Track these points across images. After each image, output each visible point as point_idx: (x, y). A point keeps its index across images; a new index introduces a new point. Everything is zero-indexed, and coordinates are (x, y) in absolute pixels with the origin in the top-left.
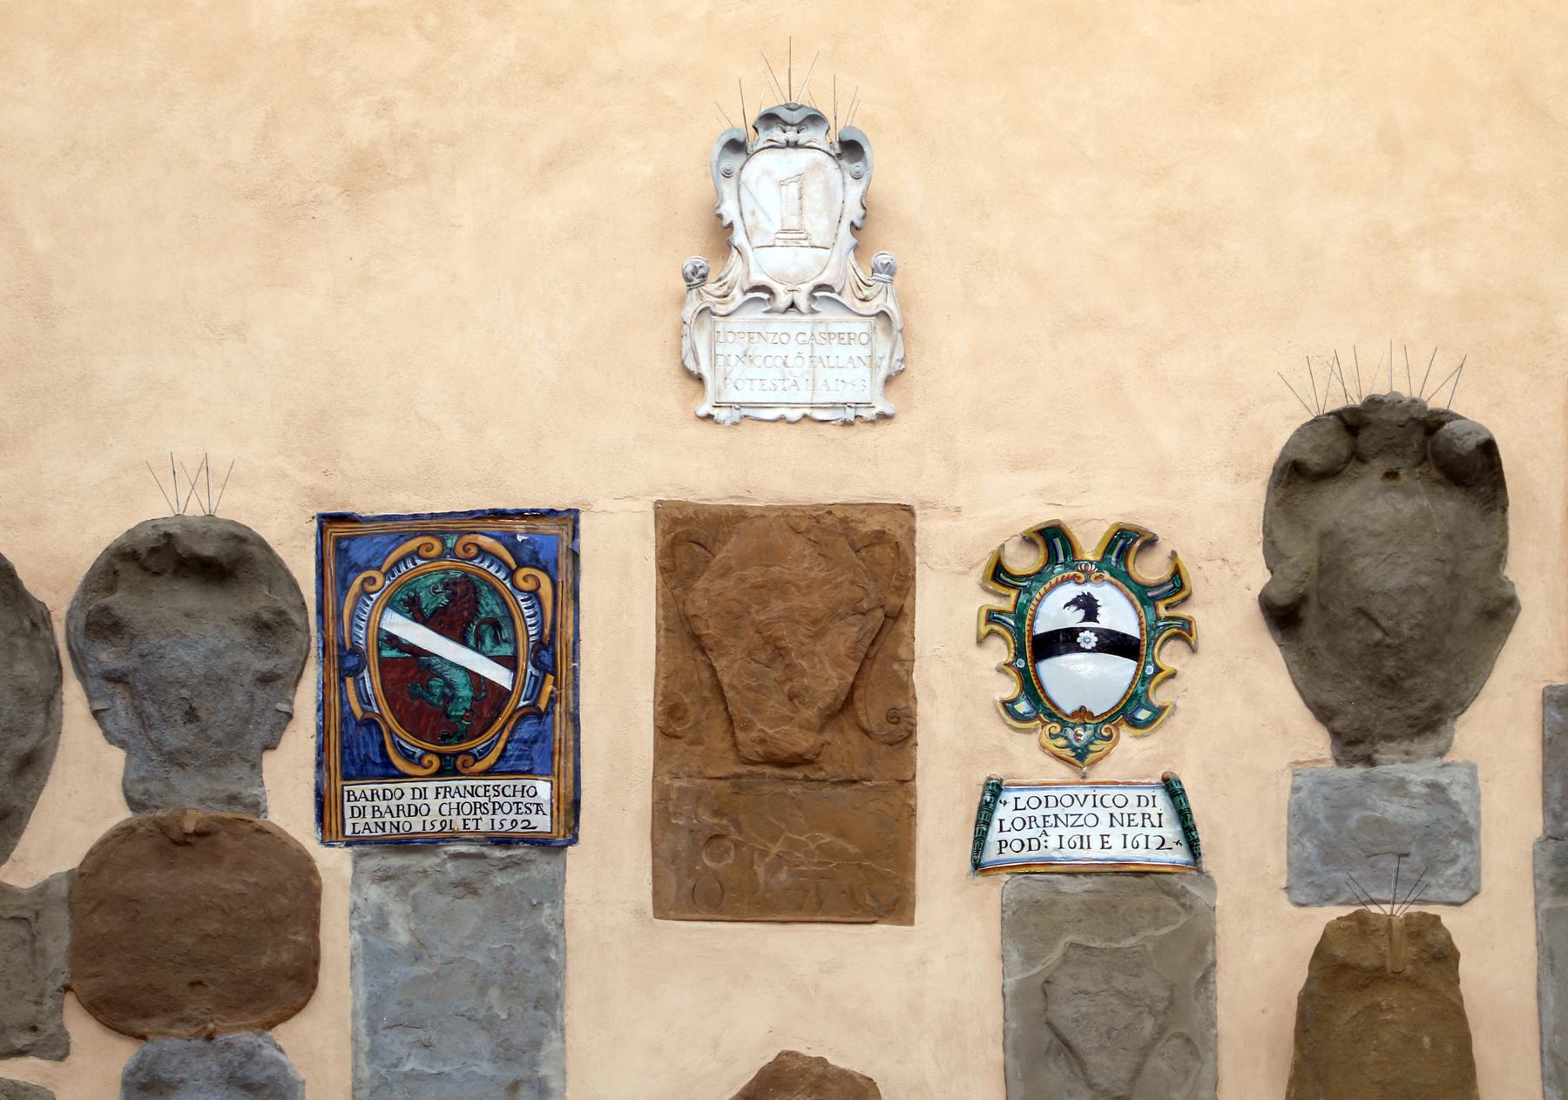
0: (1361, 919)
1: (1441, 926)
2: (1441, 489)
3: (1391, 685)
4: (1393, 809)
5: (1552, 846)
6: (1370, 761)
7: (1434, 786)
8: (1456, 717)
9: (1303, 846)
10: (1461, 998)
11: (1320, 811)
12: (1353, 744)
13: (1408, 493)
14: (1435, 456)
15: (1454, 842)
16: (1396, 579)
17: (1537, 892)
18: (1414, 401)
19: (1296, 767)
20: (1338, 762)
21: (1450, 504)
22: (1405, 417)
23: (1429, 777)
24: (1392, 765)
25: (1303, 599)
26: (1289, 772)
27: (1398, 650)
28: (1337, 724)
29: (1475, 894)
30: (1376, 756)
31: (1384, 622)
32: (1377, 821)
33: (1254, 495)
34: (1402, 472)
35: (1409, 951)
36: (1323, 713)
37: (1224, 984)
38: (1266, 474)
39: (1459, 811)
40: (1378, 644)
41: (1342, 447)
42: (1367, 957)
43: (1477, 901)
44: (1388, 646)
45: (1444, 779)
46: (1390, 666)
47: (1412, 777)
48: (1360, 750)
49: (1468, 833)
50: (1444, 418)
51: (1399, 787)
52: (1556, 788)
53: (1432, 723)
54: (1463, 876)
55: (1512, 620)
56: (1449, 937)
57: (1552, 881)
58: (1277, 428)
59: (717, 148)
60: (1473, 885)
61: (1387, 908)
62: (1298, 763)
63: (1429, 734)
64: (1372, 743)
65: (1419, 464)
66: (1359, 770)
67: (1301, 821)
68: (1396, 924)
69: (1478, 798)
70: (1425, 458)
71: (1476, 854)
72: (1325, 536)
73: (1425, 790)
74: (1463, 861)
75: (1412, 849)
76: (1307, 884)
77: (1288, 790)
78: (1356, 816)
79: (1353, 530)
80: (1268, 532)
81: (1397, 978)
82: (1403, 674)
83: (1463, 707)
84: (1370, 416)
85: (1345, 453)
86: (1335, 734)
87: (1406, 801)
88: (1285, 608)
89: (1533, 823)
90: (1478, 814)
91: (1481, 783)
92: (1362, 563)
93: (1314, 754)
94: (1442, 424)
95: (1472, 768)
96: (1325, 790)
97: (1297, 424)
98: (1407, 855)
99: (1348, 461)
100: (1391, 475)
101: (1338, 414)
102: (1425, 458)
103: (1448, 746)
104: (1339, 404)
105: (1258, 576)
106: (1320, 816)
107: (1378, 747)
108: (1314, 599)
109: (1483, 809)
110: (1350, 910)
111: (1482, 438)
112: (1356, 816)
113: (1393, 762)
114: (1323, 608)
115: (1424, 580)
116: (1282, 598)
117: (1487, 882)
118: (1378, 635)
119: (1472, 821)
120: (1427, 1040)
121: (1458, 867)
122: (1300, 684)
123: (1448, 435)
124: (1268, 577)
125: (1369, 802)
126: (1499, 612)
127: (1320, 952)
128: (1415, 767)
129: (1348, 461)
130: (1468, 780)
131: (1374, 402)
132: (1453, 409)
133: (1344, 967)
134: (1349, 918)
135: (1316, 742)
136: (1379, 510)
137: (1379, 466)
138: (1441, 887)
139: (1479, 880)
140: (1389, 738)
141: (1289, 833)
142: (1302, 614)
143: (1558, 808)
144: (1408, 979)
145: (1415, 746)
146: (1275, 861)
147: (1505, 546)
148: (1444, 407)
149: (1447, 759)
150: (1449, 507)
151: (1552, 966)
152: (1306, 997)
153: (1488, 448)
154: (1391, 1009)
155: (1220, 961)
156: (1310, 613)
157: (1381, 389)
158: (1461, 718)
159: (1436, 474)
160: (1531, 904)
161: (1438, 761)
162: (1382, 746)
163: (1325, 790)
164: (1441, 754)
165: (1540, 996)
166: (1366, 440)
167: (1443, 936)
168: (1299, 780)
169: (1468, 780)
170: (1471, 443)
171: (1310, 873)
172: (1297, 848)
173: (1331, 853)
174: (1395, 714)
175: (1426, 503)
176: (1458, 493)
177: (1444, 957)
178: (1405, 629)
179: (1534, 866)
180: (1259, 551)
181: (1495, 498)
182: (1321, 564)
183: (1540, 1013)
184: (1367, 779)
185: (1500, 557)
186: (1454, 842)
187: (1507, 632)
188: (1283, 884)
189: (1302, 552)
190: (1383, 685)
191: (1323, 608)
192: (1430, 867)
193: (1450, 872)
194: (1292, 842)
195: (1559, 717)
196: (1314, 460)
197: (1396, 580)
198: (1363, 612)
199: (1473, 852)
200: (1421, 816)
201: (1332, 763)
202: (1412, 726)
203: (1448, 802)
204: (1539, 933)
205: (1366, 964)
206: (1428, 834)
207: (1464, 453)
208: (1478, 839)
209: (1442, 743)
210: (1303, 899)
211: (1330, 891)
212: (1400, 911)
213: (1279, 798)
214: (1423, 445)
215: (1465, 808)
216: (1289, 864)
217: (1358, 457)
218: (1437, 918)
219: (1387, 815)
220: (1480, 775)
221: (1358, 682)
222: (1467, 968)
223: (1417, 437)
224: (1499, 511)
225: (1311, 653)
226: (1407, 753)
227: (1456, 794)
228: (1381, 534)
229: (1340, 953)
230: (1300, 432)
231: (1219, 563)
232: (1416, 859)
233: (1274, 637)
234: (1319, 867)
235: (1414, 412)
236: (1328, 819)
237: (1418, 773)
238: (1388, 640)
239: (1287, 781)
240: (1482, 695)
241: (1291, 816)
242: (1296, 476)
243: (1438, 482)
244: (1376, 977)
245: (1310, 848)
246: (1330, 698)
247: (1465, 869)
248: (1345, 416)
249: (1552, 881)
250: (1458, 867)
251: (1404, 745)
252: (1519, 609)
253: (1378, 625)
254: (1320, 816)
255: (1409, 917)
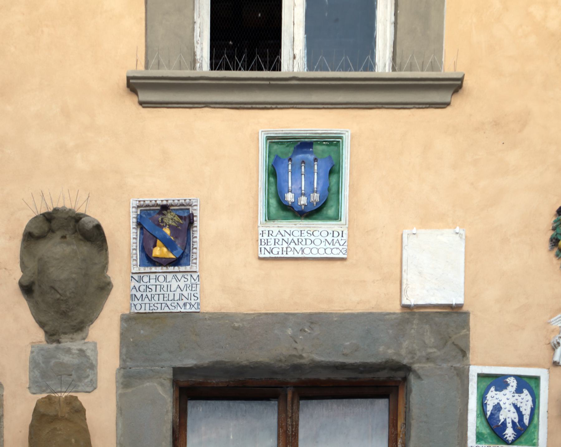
0: (49, 398)
1: (78, 400)
2: (82, 243)
3: (64, 314)
4: (66, 359)
5: (122, 371)
6: (59, 342)
7: (81, 351)
8: (89, 326)
9: (34, 372)
10: (87, 425)
11: (40, 360)
12: (52, 335)
13: (69, 244)
14: (80, 230)
15: (88, 370)
16: (64, 276)
17: (117, 387)
18: (70, 210)
19: (33, 345)
20: (47, 342)
21: (85, 248)
22: (66, 216)
23: (79, 347)
24: (66, 343)
25: (33, 283)
26: (30, 346)
27: (66, 301)
28: (46, 328)
29: (95, 388)
30: (60, 340)
31: (60, 291)
32: (61, 363)
33: (16, 244)
34: (67, 236)
35: (66, 409)
36: (42, 325)
37: (6, 422)
38: (21, 237)
39: (90, 359)
40: (58, 299)
41: (45, 227)
42: (51, 412)
43: (96, 391)
44: (62, 300)
45: (84, 348)
46: (63, 307)
47: (73, 347)
48: (55, 338)
49: (93, 367)
50: (81, 216)
51: (68, 351)
52: (124, 350)
53: (80, 327)
54: (91, 382)
55: (110, 290)
56: (81, 404)
57: (122, 383)
58: (24, 218)
59: (452, 103)
60: (94, 385)
61: (59, 394)
62: (33, 343)
63: (80, 332)
64: (59, 335)
65: (74, 233)
66: (54, 345)
67: (34, 364)
68: (61, 399)
69: (97, 355)
70: (76, 231)
71: (96, 374)
72: (40, 260)
73: (77, 352)
74: (91, 377)
75: (73, 373)
76: (35, 385)
77: (29, 352)
78: (53, 361)
79: (48, 258)
80: (21, 258)
81: (62, 419)
82: (68, 310)
83: (92, 322)
84: (54, 215)
85: (47, 229)
86: (46, 332)
87: (71, 356)
88: (27, 286)
89: (116, 363)
90: (97, 360)
91: (98, 349)
92: (52, 270)
93: (38, 339)
94: (81, 218)
95: (95, 344)
96: (42, 352)
97: (31, 218)
98: (71, 375)
99: (48, 232)
100: (64, 237)
101: (44, 215)
102: (76, 231)
103: (87, 336)
104: (44, 211)
105: (18, 274)
106: (41, 362)
107: (61, 336)
108: (37, 283)
109: (99, 358)
110: (45, 395)
111: (95, 223)
112: (53, 361)
113: (66, 342)
114: (40, 286)
115: (74, 276)
116: (25, 283)
117: (99, 384)
118: (58, 296)
119: (94, 362)
120: (73, 440)
121: (89, 379)
122: (34, 314)
123: (83, 223)
124: (22, 274)
125: (58, 356)
126: (105, 288)
127: (35, 410)
128: (75, 344)
129: (48, 232)
130: (93, 348)
131: (56, 210)
132: (87, 214)
133: (43, 415)
134: (45, 398)
135: (40, 335)
136: (56, 249)
137: (59, 234)
138: (83, 386)
139: (97, 384)
140: (65, 333)
141: (30, 368)
142: (33, 288)
143: (125, 357)
144: (66, 419)
145: (75, 336)
146: (25, 378)
147: (107, 263)
148: (84, 212)
149: (86, 341)
150: (85, 249)
151: (121, 413)
152: (31, 426)
153: (98, 227)
154: (60, 430)
155: (5, 414)
156: (36, 288)
157: (60, 206)
158: (92, 326)
159: (80, 237)
160: (115, 391)
161: (83, 341)
162: (62, 336)
163: (42, 352)
164: (84, 339)
165: (117, 424)
166: (54, 224)
167: (78, 403)
168: (33, 349)
169: (93, 348)
170: (91, 225)
171: (37, 382)
172: (32, 373)
173: (44, 375)
174: (66, 324)
175: (75, 247)
176: (89, 244)
177: (80, 411)
178: (68, 294)
179: (116, 378)
180: (19, 265)
181: (103, 246)
182: (38, 270)
183: (117, 430)
184: (57, 348)
185: (105, 267)
186: (88, 370)
187: (108, 294)
188: (28, 386)
189: (33, 265)
190: (61, 314)
191: (40, 286)
192: (80, 379)
193: (86, 381)
194: (31, 371)
195: (126, 325)
196: (36, 232)
197: (64, 276)
198: (52, 288)
199: (94, 374)
200: (76, 361)
201: (45, 343)
202: (73, 329)
203: (86, 356)
204: (117, 402)
205: (51, 414)
206: (79, 368)
207: (88, 229)
208: (97, 369)
209: (84, 335)
210: (34, 391)
211: (44, 388)
212: (64, 395)
213: (26, 356)
214: (75, 226)
215: (92, 358)
216: (30, 379)
217: (51, 230)
218: (77, 397)
219: (64, 361)
220: (98, 346)
221: (53, 313)
222: (89, 414)
223: (72, 223)
224: (104, 251)
225: (37, 303)
226: (72, 339)
227: (89, 353)
228: (58, 259)
229: (42, 410)
230: (31, 221)
231: (4, 270)
232: (74, 376)
233: (24, 297)
234: (40, 380)
235: (70, 214)
236: (43, 363)
237: (75, 346)
238: (62, 298)
239: (29, 349)
240: (99, 317)
241: (30, 362)
242: (31, 238)
243: (81, 240)
244: (55, 418)
245: (37, 373)
246: (44, 319)
247: (91, 380)
248: (46, 215)
249: (122, 383)
250: (89, 379)
251: (71, 336)
252: (112, 286)
253: (58, 292)
254: (41, 362)
255: (66, 397)
